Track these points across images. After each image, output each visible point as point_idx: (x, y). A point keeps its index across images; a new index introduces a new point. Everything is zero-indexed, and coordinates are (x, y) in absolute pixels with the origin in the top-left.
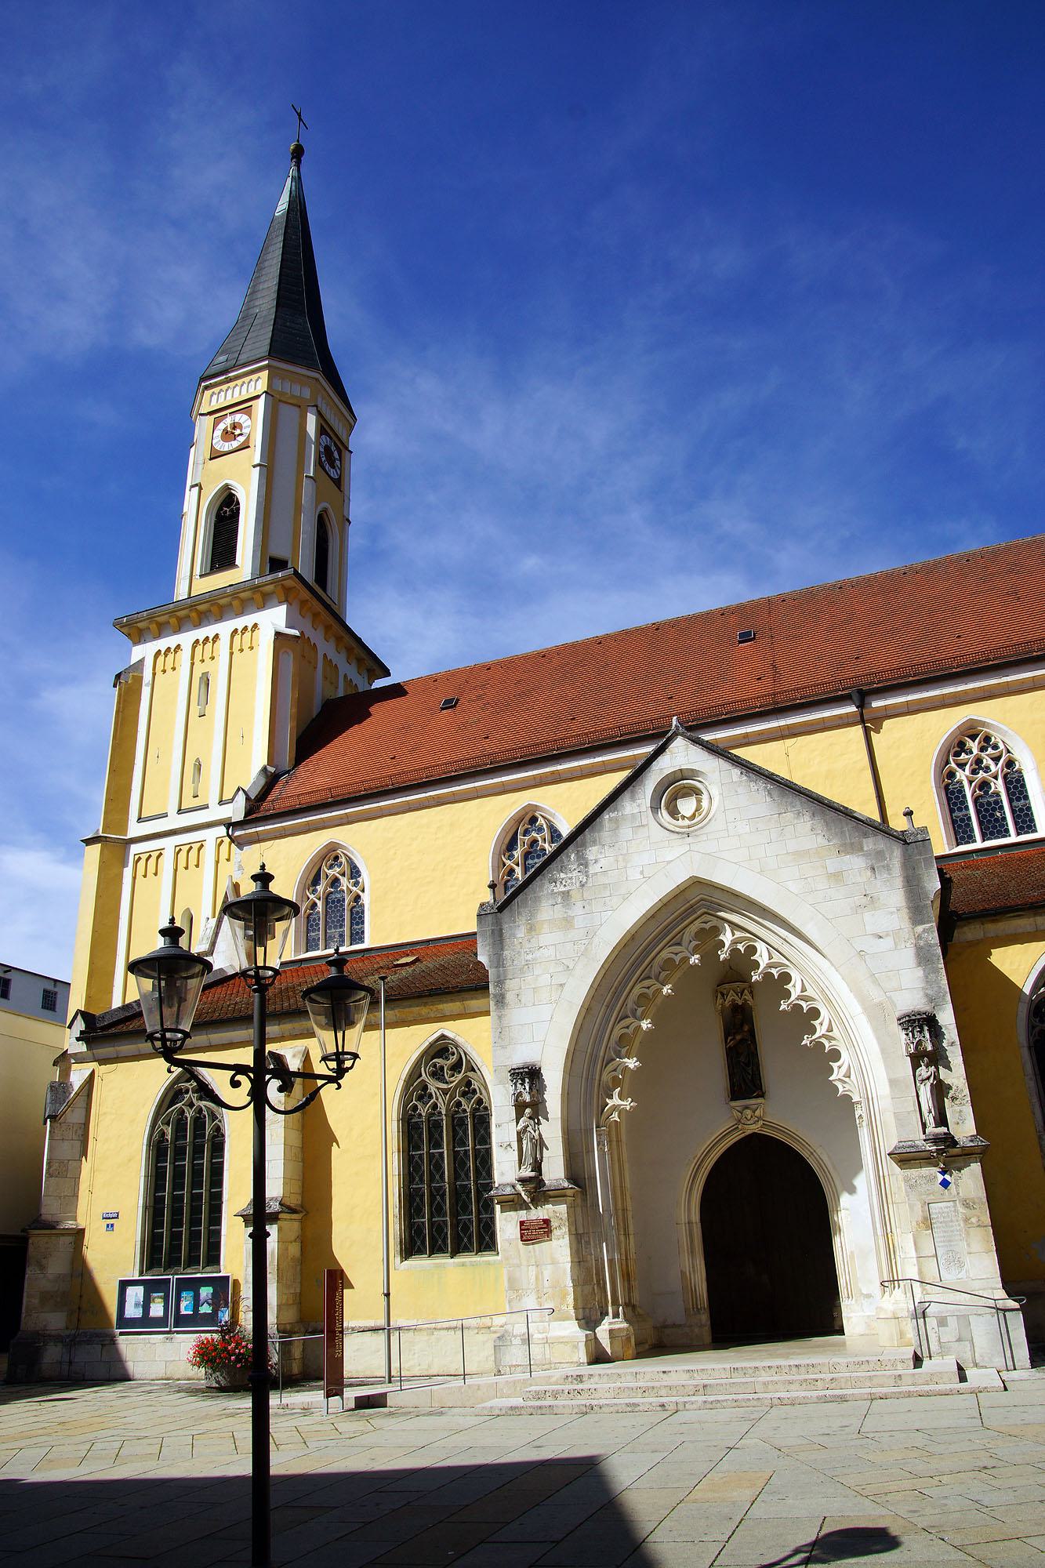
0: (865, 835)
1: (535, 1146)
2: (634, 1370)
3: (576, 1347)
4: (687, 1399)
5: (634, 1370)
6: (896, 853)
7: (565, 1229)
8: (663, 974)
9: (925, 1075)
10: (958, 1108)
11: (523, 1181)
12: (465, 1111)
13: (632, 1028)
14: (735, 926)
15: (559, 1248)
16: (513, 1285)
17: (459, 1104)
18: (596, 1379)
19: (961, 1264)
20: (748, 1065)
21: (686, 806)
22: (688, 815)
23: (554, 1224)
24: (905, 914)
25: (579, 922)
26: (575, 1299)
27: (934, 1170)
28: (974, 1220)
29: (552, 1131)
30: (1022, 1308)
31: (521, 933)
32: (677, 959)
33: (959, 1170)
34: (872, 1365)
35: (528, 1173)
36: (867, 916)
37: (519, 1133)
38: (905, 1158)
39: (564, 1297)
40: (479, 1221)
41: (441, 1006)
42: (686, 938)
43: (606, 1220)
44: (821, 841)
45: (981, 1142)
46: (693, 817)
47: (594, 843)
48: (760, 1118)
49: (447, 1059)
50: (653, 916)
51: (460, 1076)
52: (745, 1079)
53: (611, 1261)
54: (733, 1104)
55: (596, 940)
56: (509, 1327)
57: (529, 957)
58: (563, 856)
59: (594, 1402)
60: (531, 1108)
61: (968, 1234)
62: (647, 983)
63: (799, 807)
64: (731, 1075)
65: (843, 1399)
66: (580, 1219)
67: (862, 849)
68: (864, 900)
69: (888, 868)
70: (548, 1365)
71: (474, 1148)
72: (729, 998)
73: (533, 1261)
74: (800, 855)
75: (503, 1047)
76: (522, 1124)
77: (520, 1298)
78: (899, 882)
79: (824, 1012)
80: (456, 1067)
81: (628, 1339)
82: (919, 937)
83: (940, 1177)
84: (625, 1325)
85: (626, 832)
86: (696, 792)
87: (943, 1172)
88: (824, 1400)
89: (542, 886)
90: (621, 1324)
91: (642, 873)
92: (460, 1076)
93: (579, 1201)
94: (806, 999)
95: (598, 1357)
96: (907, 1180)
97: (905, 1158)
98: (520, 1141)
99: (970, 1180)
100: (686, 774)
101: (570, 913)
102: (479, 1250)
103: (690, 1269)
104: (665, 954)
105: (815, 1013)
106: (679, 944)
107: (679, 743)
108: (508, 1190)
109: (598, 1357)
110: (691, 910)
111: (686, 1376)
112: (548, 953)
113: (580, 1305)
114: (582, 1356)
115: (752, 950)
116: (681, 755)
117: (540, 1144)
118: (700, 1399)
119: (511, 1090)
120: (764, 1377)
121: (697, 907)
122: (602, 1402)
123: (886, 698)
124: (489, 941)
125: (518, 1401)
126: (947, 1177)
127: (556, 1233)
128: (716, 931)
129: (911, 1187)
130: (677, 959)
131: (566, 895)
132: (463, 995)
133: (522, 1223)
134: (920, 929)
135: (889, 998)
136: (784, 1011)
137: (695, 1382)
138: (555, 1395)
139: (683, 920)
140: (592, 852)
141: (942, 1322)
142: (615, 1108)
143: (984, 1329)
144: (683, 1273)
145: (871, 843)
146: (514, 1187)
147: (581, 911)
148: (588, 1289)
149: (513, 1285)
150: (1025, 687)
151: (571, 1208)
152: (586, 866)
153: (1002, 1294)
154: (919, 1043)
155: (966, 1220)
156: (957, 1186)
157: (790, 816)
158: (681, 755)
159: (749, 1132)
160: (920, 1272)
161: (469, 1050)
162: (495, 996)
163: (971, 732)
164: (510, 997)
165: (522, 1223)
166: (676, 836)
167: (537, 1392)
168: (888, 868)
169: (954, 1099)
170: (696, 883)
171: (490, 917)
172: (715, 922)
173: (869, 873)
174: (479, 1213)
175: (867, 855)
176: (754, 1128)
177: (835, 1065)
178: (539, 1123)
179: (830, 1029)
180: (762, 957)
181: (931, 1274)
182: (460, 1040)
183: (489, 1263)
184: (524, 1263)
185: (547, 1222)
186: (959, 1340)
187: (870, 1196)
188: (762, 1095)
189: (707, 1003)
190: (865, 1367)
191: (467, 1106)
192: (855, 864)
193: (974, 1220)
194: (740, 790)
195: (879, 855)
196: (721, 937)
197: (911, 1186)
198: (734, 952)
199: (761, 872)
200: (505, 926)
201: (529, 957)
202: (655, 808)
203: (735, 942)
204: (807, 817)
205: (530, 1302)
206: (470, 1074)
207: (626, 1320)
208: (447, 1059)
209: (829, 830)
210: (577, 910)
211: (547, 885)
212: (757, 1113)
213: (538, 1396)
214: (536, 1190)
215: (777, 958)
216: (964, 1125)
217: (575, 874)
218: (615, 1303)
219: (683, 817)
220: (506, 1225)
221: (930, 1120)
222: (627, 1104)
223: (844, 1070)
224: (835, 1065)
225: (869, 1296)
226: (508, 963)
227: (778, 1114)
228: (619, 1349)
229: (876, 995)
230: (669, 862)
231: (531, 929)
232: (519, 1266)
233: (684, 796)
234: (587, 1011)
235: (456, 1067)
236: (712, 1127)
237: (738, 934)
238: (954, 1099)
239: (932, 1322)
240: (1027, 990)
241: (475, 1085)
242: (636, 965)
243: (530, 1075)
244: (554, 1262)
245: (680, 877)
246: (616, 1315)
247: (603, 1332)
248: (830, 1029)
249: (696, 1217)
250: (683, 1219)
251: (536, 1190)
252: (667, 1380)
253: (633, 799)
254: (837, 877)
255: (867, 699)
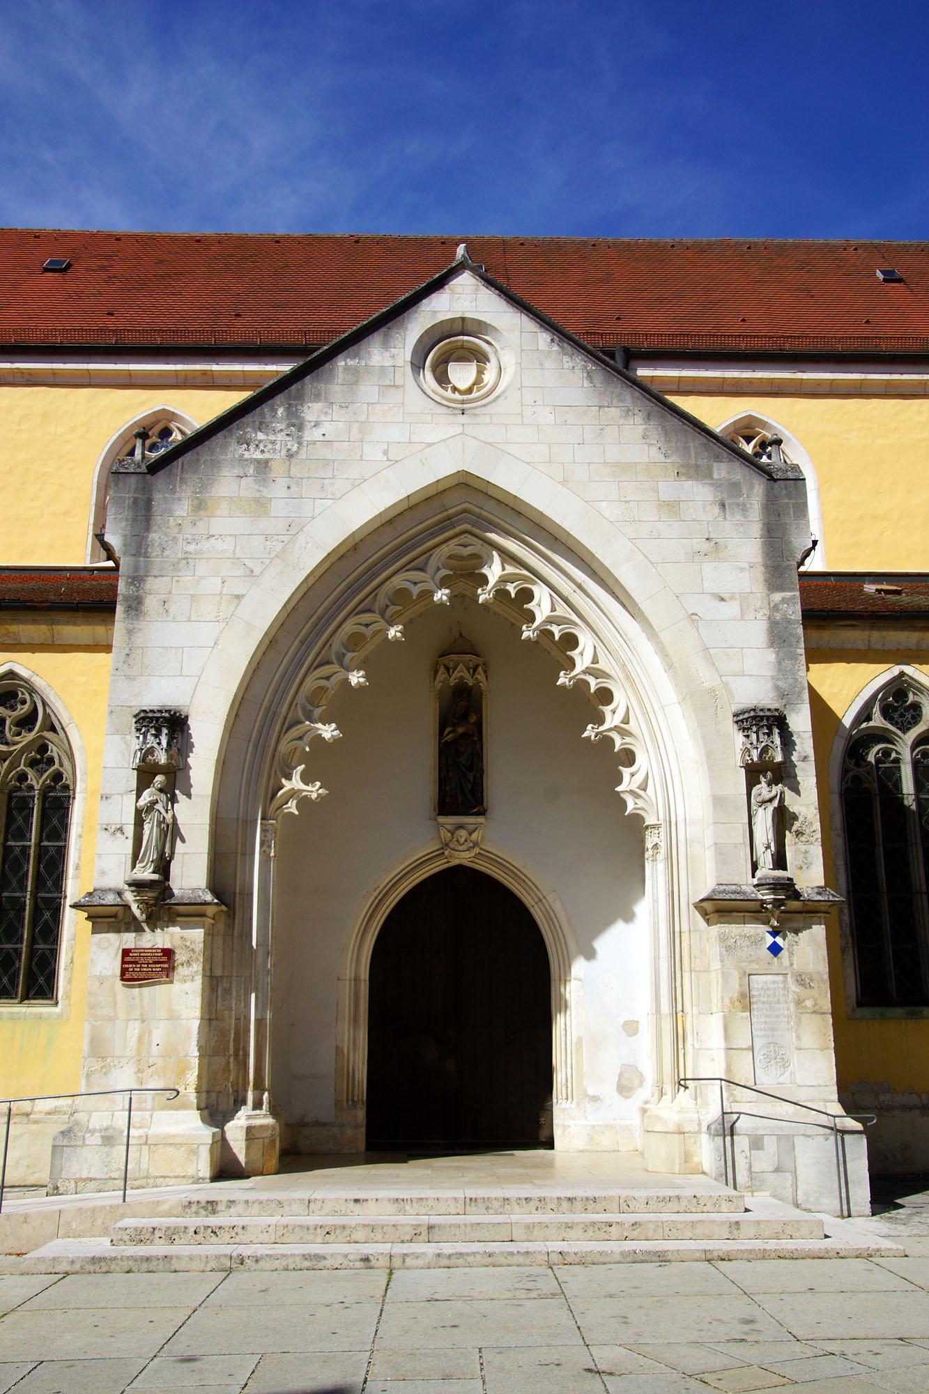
0: (717, 458)
1: (163, 834)
2: (305, 1195)
3: (194, 1152)
4: (399, 1249)
5: (305, 1195)
6: (757, 490)
7: (197, 967)
8: (392, 609)
9: (767, 796)
10: (803, 847)
11: (138, 886)
12: (31, 788)
13: (334, 679)
14: (508, 557)
15: (184, 996)
16: (98, 1049)
17: (23, 777)
18: (240, 1208)
19: (784, 1064)
20: (470, 769)
21: (462, 374)
22: (463, 386)
23: (180, 957)
24: (759, 573)
25: (279, 508)
26: (199, 1077)
27: (762, 929)
28: (809, 1003)
29: (194, 814)
30: (867, 1132)
31: (182, 509)
32: (415, 590)
33: (796, 932)
34: (684, 1203)
35: (146, 873)
36: (707, 568)
37: (138, 812)
38: (720, 908)
39: (182, 1072)
40: (32, 952)
41: (14, 628)
42: (433, 563)
43: (260, 959)
44: (655, 454)
45: (831, 896)
46: (470, 391)
47: (317, 397)
48: (476, 844)
49: (13, 708)
50: (390, 522)
51: (32, 736)
52: (460, 789)
53: (260, 1022)
54: (442, 819)
55: (301, 539)
56: (81, 1117)
57: (191, 548)
58: (266, 408)
59: (246, 1251)
60: (162, 774)
61: (799, 1022)
62: (366, 617)
63: (629, 403)
64: (442, 782)
65: (662, 1258)
66: (219, 953)
67: (710, 476)
68: (706, 546)
69: (743, 508)
70: (148, 1180)
71: (38, 845)
72: (456, 675)
73: (137, 1014)
74: (623, 468)
75: (129, 678)
76: (147, 797)
77: (106, 1070)
78: (756, 529)
79: (618, 696)
80: (27, 722)
81: (273, 1142)
82: (776, 608)
83: (770, 940)
84: (270, 1121)
85: (368, 390)
86: (479, 357)
87: (775, 933)
88: (634, 1258)
89: (225, 447)
90: (264, 1119)
91: (386, 452)
92: (32, 736)
93: (221, 926)
94: (597, 674)
95: (226, 1170)
96: (723, 939)
97: (720, 908)
98: (139, 824)
99: (810, 948)
100: (469, 327)
101: (265, 493)
102: (26, 997)
103: (347, 1043)
104: (349, 627)
105: (606, 696)
106: (422, 570)
107: (465, 280)
108: (110, 899)
109: (226, 1170)
110: (448, 522)
111: (393, 1208)
112: (226, 546)
113: (204, 1088)
114: (204, 1167)
115: (526, 595)
116: (465, 297)
117: (171, 832)
118: (430, 1249)
119: (135, 743)
120: (519, 1216)
121: (458, 516)
122: (261, 1250)
123: (655, 368)
124: (128, 514)
125: (100, 1245)
126: (779, 940)
127: (181, 971)
128: (481, 560)
129: (728, 948)
130: (415, 590)
131: (263, 466)
132: (54, 615)
133: (126, 952)
134: (777, 597)
135: (726, 684)
136: (563, 687)
137: (413, 1220)
138: (171, 1236)
139: (433, 535)
140: (312, 411)
141: (757, 1143)
142: (293, 793)
143: (814, 1156)
144: (339, 1050)
145: (724, 470)
146: (120, 894)
147: (283, 492)
148: (219, 1061)
149: (98, 1049)
150: (821, 390)
151: (210, 935)
152: (300, 428)
153: (837, 1109)
154: (765, 750)
155: (799, 1002)
156: (791, 953)
157: (614, 412)
158: (465, 297)
159: (455, 862)
160: (728, 1069)
161: (51, 698)
162: (126, 598)
163: (747, 432)
164: (151, 603)
165: (126, 952)
166: (444, 410)
167: (139, 1231)
168: (743, 508)
169: (799, 833)
170: (465, 485)
171: (133, 480)
172: (476, 547)
173: (717, 510)
174: (33, 941)
175: (716, 485)
176: (463, 858)
177: (626, 772)
178: (173, 800)
179: (626, 721)
180: (542, 605)
181: (744, 1075)
182: (38, 682)
183: (39, 1017)
184: (122, 1015)
185: (169, 953)
186: (777, 1170)
187: (656, 959)
188: (482, 813)
189: (443, 670)
190: (673, 1206)
191: (36, 781)
192: (698, 495)
193: (809, 1003)
194: (548, 364)
195: (734, 488)
196: (485, 570)
197: (728, 947)
198: (501, 594)
199: (564, 482)
200: (157, 497)
201: (191, 548)
202: (418, 366)
203: (504, 580)
204: (639, 419)
205: (124, 1077)
206: (46, 734)
207: (274, 1111)
208: (13, 708)
209: (668, 441)
210: (277, 490)
211: (233, 445)
212: (474, 836)
213: (139, 1237)
214: (159, 901)
215: (563, 610)
216: (810, 870)
217: (281, 437)
218: (259, 1086)
219: (455, 389)
220: (85, 954)
221: (766, 860)
222: (314, 790)
223: (639, 779)
224: (626, 772)
225: (595, 1099)
226: (155, 552)
227: (512, 843)
228: (257, 1154)
229: (708, 678)
230: (430, 445)
231: (200, 506)
232: (112, 1019)
233: (458, 360)
234: (271, 644)
235: (27, 722)
236: (406, 847)
237: (510, 569)
238: (799, 833)
239: (742, 1142)
240: (847, 722)
241: (53, 751)
242: (353, 589)
243: (172, 725)
244: (173, 1017)
245: (441, 468)
246: (258, 1105)
247: (236, 1130)
248: (626, 721)
249: (365, 974)
250: (349, 973)
251: (159, 901)
252: (366, 1215)
253: (386, 345)
254: (672, 507)
255: (633, 364)
